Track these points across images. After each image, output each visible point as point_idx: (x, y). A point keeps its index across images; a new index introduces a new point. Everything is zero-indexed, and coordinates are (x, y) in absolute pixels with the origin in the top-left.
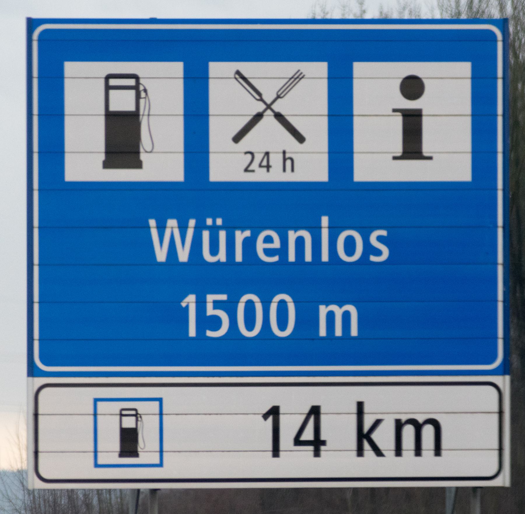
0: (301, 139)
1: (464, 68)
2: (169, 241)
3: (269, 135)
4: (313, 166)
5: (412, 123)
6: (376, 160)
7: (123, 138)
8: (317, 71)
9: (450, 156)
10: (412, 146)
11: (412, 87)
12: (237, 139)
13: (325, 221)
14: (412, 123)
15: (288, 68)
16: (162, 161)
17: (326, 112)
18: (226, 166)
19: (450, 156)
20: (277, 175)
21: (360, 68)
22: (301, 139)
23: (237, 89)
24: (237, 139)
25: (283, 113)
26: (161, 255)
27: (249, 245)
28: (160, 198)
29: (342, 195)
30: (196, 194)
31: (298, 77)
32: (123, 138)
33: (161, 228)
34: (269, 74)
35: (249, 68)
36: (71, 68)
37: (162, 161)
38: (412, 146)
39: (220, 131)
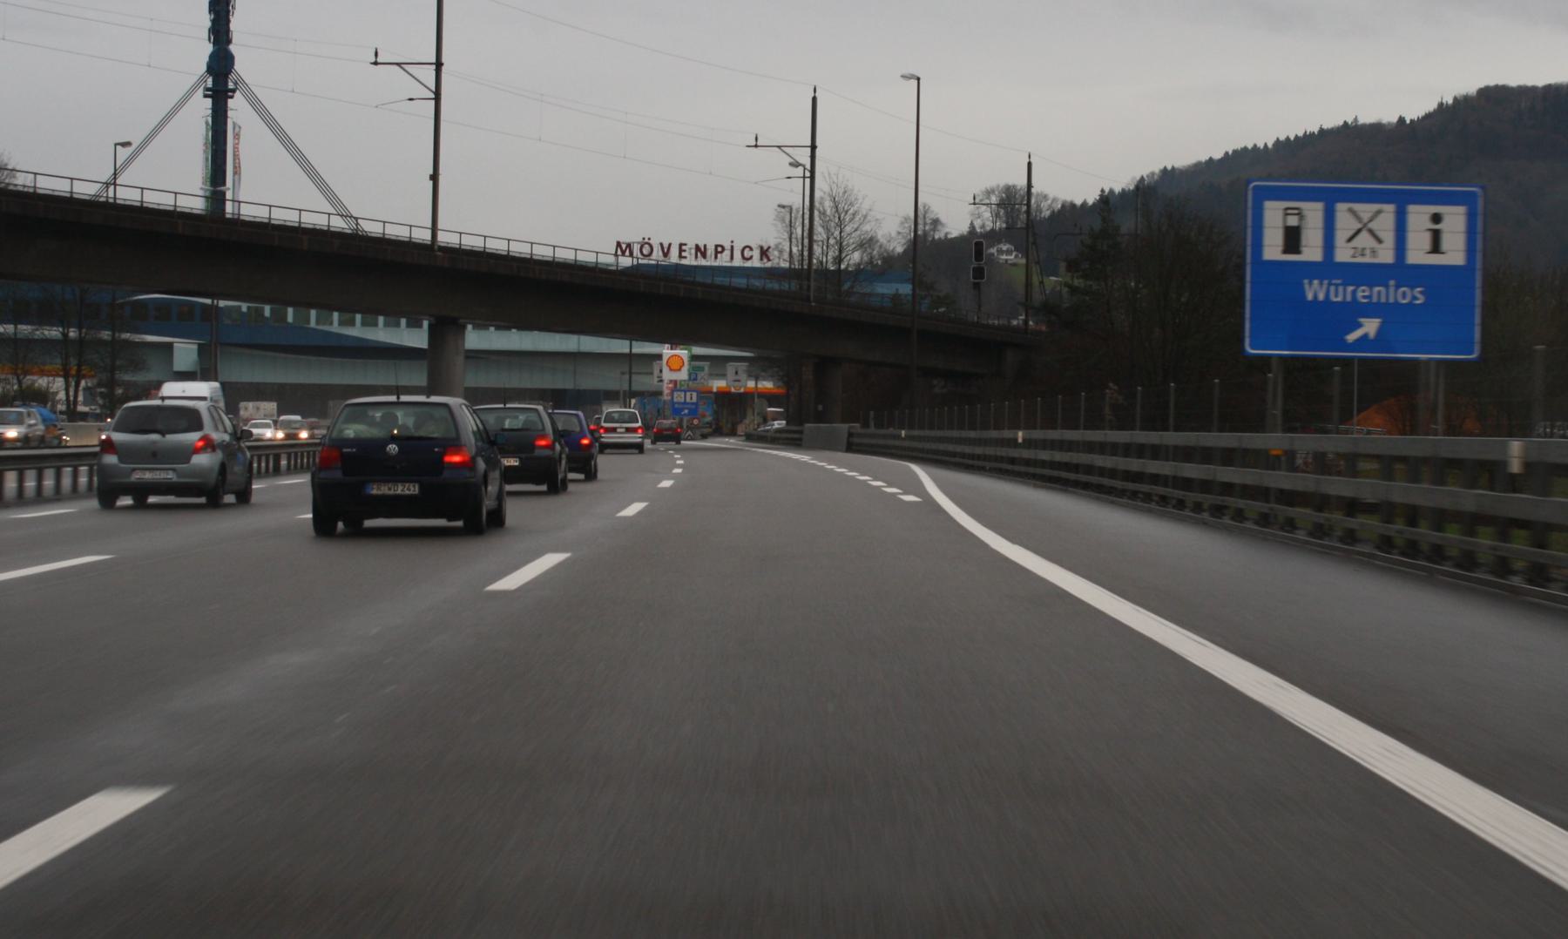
0: (1380, 241)
1: (1461, 210)
2: (1314, 290)
3: (1364, 240)
4: (1386, 256)
5: (1436, 236)
6: (1418, 253)
7: (1292, 239)
8: (1389, 209)
9: (1454, 253)
10: (1436, 248)
11: (1437, 218)
12: (1350, 240)
13: (1392, 283)
14: (1436, 236)
15: (1375, 207)
16: (1419, 216)
17: (444, 238)
18: (1343, 255)
19: (1454, 253)
20: (1367, 259)
21: (1412, 208)
22: (1380, 241)
23: (1348, 216)
24: (1350, 240)
25: (239, 66)
26: (1310, 297)
27: (1354, 292)
28: (1311, 270)
29: (1400, 271)
30: (1328, 268)
31: (1379, 212)
32: (1292, 239)
33: (1310, 284)
34: (1366, 210)
35: (1357, 207)
36: (1268, 204)
37: (1312, 251)
38: (1436, 248)
39: (1341, 236)
